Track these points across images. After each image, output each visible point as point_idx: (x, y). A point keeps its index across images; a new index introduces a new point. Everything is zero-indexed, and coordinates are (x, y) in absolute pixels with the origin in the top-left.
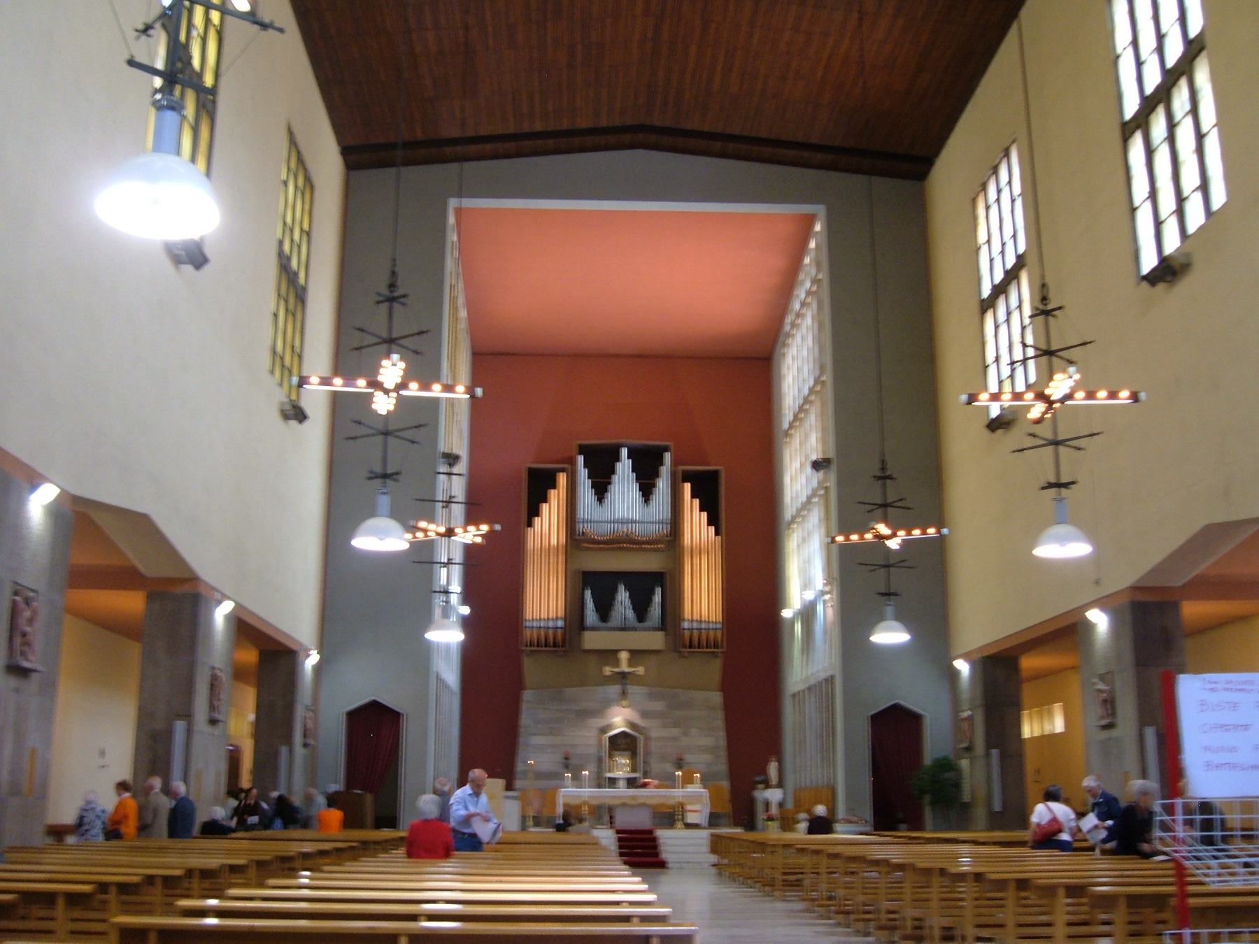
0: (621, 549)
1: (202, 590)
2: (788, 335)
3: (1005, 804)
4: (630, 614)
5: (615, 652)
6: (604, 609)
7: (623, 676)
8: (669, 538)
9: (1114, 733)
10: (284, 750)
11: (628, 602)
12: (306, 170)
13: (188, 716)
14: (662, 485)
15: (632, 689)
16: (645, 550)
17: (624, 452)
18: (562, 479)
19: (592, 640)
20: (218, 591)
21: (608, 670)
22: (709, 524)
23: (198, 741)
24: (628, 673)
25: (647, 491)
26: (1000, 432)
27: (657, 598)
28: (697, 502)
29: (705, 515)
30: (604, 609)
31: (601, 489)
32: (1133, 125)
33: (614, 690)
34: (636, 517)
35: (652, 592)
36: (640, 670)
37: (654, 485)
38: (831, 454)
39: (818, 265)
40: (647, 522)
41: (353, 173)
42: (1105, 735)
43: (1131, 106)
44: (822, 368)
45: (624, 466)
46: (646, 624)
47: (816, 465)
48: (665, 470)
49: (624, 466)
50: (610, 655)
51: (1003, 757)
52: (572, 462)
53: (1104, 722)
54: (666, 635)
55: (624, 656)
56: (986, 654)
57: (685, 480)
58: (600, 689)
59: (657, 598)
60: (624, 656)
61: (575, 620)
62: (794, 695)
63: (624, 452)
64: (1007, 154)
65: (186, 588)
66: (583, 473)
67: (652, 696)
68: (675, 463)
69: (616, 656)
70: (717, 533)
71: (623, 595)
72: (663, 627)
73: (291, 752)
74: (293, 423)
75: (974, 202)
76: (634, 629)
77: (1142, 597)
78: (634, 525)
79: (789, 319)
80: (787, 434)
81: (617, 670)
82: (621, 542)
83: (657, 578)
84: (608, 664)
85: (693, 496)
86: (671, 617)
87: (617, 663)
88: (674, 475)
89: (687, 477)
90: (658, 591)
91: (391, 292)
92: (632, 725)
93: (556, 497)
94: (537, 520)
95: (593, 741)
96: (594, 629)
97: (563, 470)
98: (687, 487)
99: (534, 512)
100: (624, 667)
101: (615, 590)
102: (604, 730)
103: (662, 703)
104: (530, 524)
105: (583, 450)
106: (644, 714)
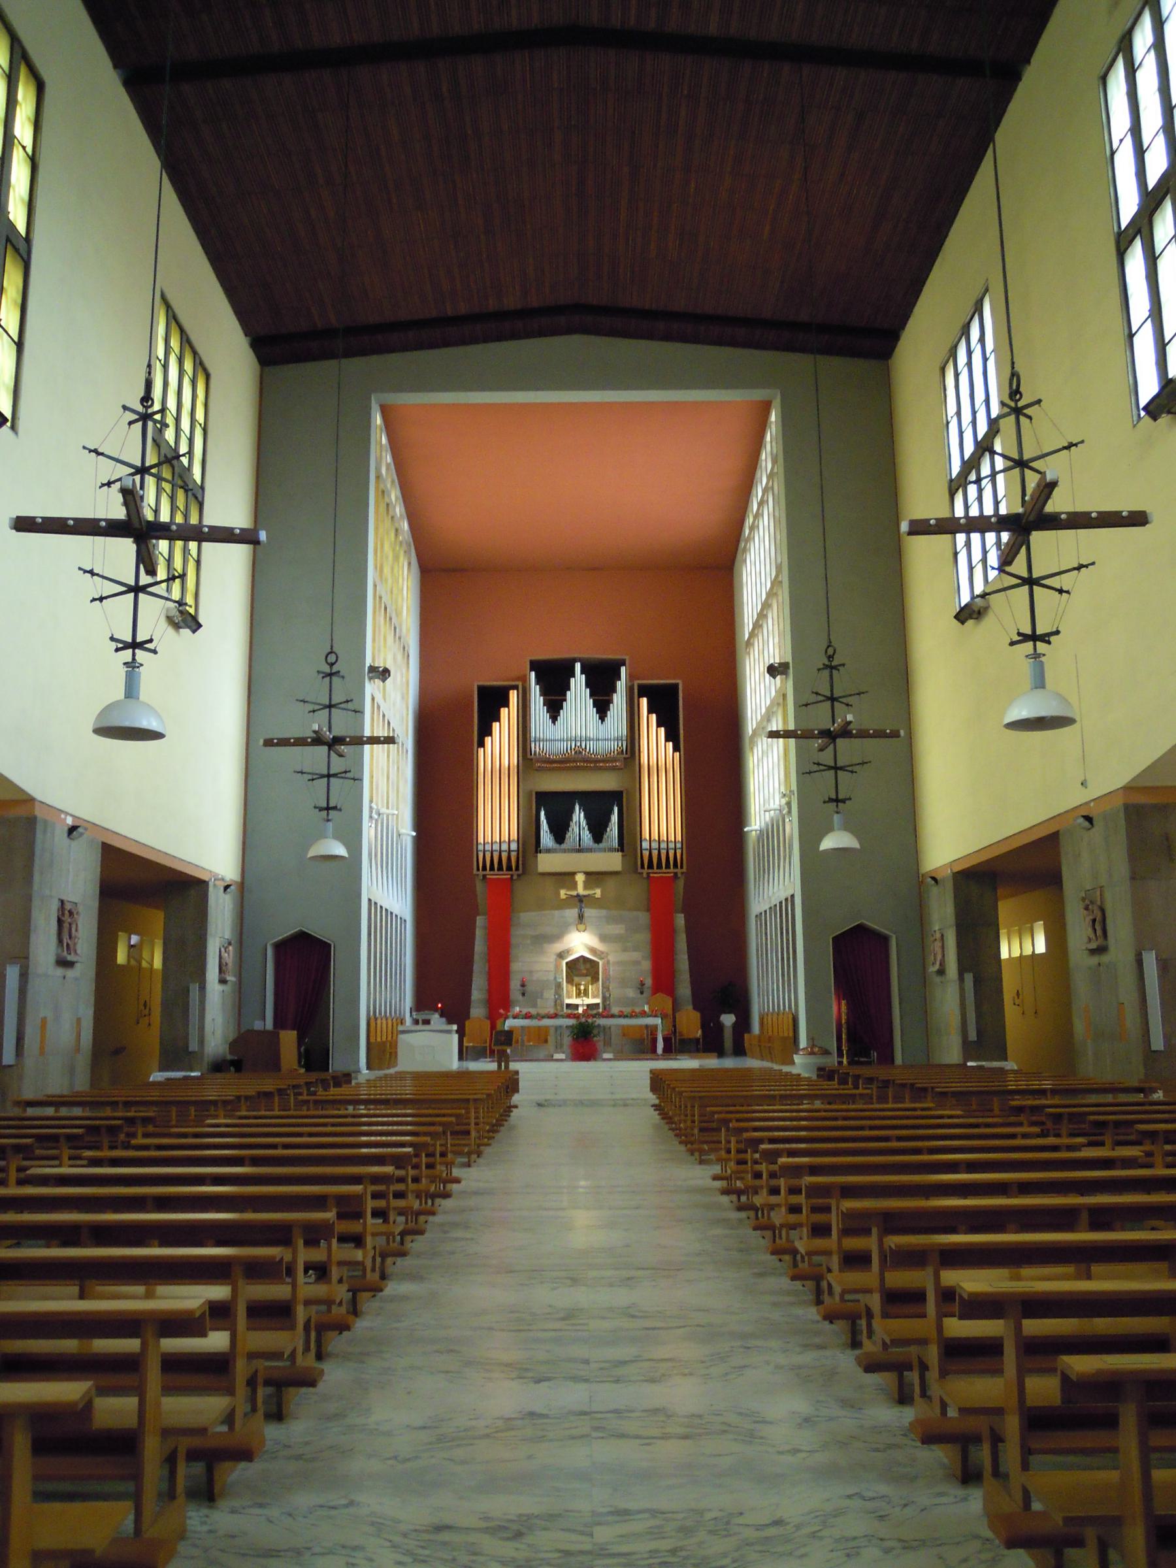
0: (578, 768)
1: (38, 812)
2: (748, 540)
3: (979, 1033)
4: (587, 836)
5: (573, 874)
6: (560, 831)
7: (580, 899)
8: (625, 756)
9: (1105, 959)
10: (194, 988)
11: (584, 823)
12: (195, 353)
13: (23, 959)
14: (619, 700)
15: (589, 912)
16: (600, 768)
17: (578, 666)
18: (513, 696)
19: (547, 862)
20: (67, 814)
21: (563, 893)
22: (667, 740)
23: (37, 986)
24: (585, 896)
25: (602, 708)
26: (970, 623)
27: (615, 818)
28: (654, 717)
29: (662, 730)
30: (560, 831)
31: (554, 708)
32: (1131, 231)
33: (572, 913)
34: (591, 734)
35: (611, 812)
36: (598, 892)
37: (611, 701)
38: (789, 658)
39: (774, 462)
40: (602, 740)
41: (267, 369)
42: (1095, 960)
43: (1129, 205)
44: (779, 569)
45: (578, 682)
46: (563, 846)
47: (772, 670)
48: (621, 685)
49: (578, 682)
50: (566, 878)
51: (977, 982)
52: (525, 679)
53: (1094, 945)
54: (623, 856)
55: (580, 878)
56: (957, 869)
57: (640, 696)
58: (556, 913)
59: (615, 818)
60: (580, 878)
61: (530, 844)
62: (758, 916)
63: (578, 666)
64: (978, 309)
65: (21, 811)
66: (535, 690)
67: (610, 920)
68: (631, 677)
69: (574, 878)
70: (676, 749)
71: (579, 816)
72: (621, 847)
73: (203, 988)
74: (186, 632)
75: (943, 370)
76: (590, 850)
77: (1142, 799)
78: (592, 742)
79: (749, 520)
80: (749, 643)
81: (574, 893)
82: (577, 761)
83: (616, 797)
84: (563, 888)
85: (650, 712)
86: (628, 841)
87: (574, 886)
88: (630, 690)
89: (644, 691)
90: (616, 809)
91: (147, 408)
92: (593, 950)
93: (509, 715)
94: (488, 740)
95: (552, 967)
96: (548, 851)
97: (515, 687)
98: (644, 701)
99: (485, 731)
100: (581, 890)
101: (571, 811)
102: (561, 956)
103: (620, 926)
104: (481, 744)
105: (535, 666)
106: (603, 938)
